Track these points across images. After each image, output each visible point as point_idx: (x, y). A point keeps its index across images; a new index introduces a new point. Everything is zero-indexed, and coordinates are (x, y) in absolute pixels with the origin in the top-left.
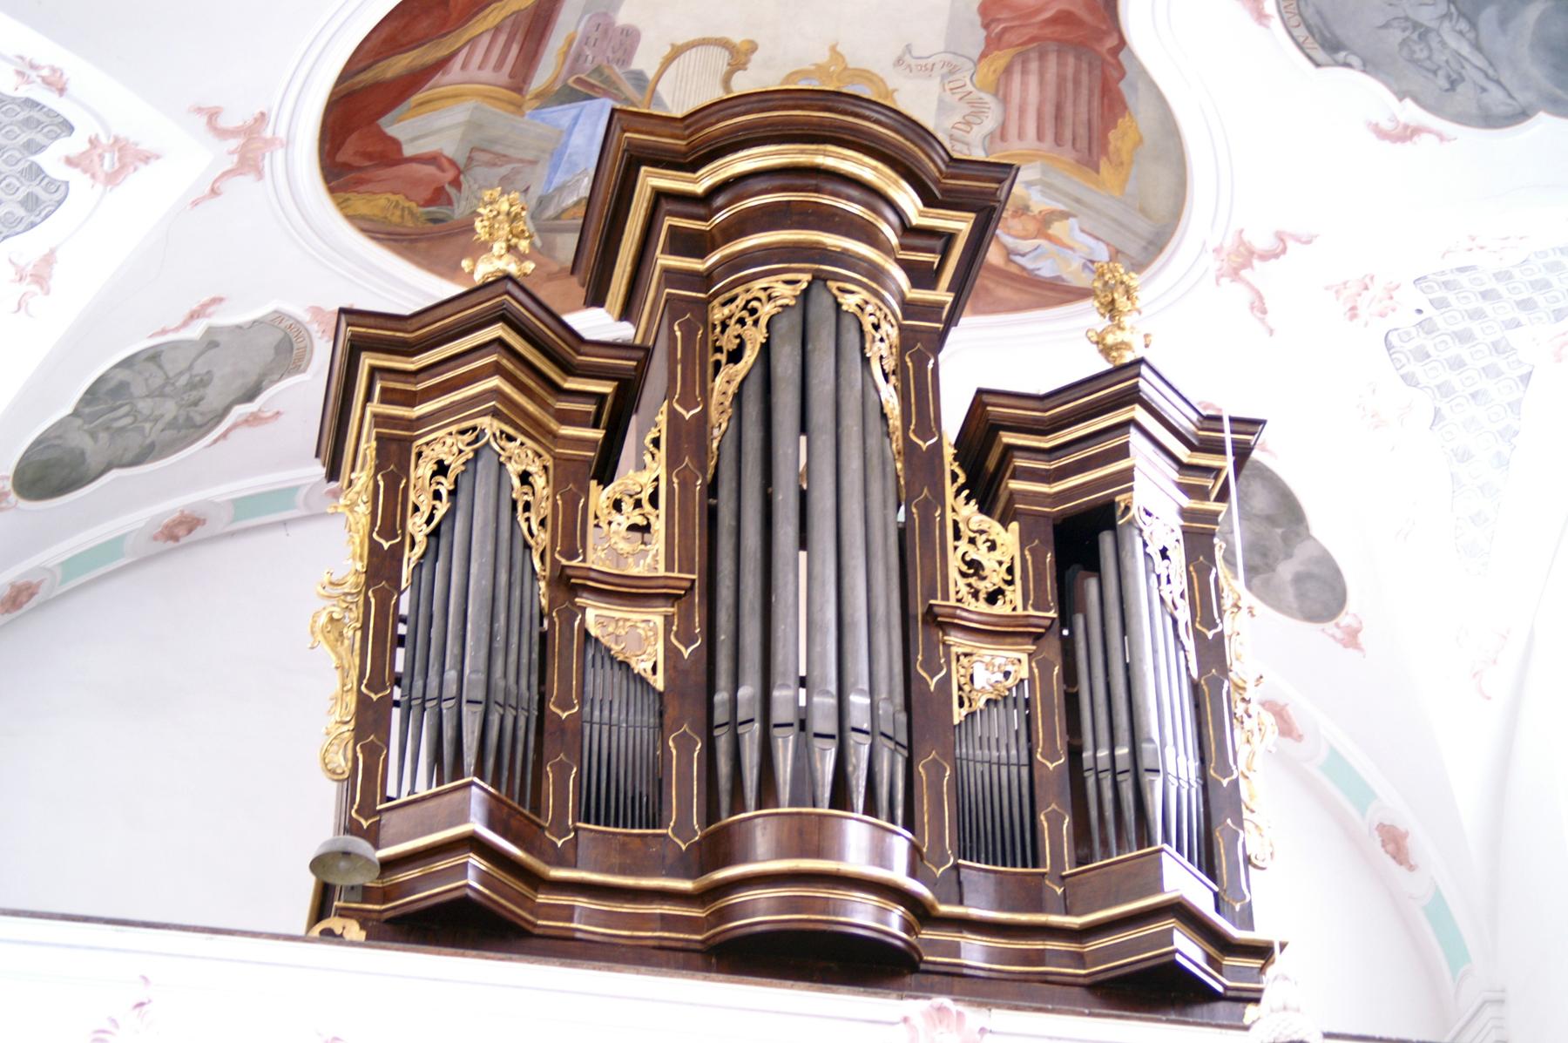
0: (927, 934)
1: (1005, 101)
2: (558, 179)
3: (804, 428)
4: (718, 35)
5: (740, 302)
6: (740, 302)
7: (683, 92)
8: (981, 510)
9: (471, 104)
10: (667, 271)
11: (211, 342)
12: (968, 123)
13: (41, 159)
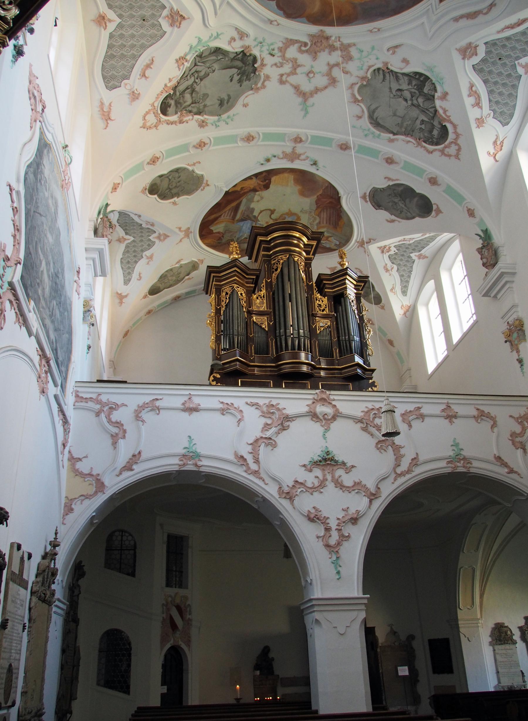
0: (315, 371)
1: (320, 218)
2: (241, 234)
3: (289, 280)
5: (277, 260)
6: (277, 260)
7: (263, 221)
8: (320, 295)
9: (225, 223)
10: (263, 255)
11: (181, 266)
13: (150, 238)
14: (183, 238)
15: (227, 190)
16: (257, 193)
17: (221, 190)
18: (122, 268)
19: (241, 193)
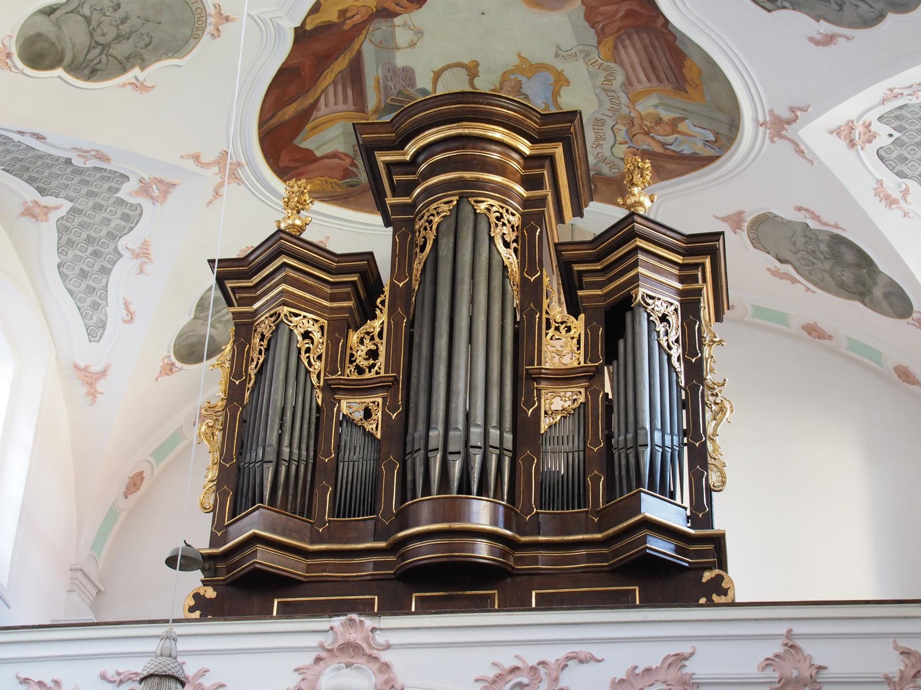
1: (621, 64)
4: (455, 61)
5: (425, 218)
6: (425, 218)
12: (609, 80)
14: (221, 185)
15: (298, 24)
16: (398, 20)
17: (278, 29)
18: (72, 293)
19: (346, 27)
